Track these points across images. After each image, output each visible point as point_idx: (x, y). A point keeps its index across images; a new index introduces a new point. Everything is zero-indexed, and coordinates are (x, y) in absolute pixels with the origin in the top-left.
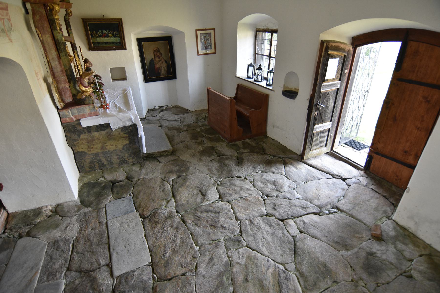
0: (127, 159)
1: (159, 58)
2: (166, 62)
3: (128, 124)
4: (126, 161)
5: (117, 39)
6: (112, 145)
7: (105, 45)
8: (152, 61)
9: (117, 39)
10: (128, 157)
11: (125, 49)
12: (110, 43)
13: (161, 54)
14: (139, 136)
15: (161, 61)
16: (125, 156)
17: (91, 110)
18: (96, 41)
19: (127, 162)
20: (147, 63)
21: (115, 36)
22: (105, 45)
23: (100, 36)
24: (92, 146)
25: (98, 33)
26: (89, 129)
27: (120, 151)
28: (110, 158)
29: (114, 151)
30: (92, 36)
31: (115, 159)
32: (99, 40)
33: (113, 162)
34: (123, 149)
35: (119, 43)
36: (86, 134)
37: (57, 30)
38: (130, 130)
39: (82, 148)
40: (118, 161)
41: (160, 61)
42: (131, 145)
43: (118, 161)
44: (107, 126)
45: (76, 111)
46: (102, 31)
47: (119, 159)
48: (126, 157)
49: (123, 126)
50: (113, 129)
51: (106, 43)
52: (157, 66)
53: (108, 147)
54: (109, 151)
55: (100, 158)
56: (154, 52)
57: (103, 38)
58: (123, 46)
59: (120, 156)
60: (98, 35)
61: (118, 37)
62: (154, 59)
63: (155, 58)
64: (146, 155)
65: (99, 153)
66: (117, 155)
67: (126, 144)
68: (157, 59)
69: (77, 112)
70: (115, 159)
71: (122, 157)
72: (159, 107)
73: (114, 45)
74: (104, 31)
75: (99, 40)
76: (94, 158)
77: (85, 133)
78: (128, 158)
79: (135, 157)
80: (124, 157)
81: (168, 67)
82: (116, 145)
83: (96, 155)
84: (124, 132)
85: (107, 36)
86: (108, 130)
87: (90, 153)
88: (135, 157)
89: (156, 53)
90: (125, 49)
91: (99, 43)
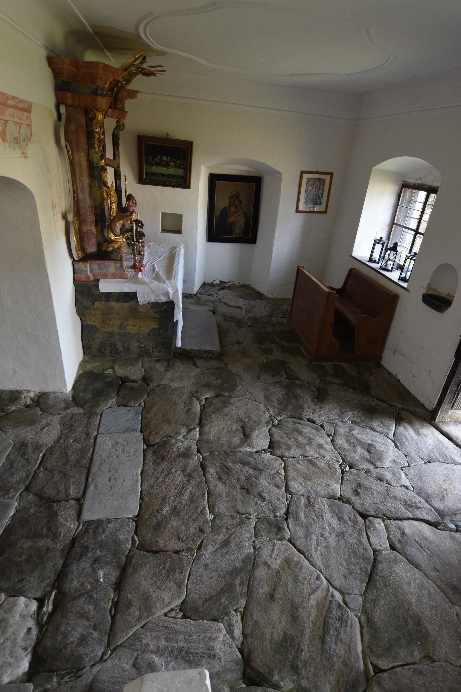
0: (151, 351)
1: (236, 208)
2: (245, 215)
3: (163, 299)
4: (149, 353)
5: (180, 172)
6: (134, 326)
7: (161, 178)
8: (224, 212)
9: (180, 172)
10: (152, 348)
11: (188, 187)
12: (169, 176)
13: (240, 202)
14: (175, 320)
15: (238, 213)
16: (149, 346)
17: (116, 269)
18: (150, 171)
19: (149, 355)
20: (217, 212)
21: (178, 167)
22: (161, 178)
23: (157, 165)
24: (108, 321)
25: (156, 159)
26: (108, 296)
27: (144, 336)
28: (128, 344)
29: (136, 334)
30: (146, 163)
31: (134, 346)
32: (155, 169)
33: (131, 350)
34: (149, 334)
35: (182, 177)
36: (103, 302)
37: (95, 148)
38: (164, 309)
39: (94, 321)
40: (139, 350)
41: (236, 212)
42: (161, 331)
43: (139, 350)
44: (132, 297)
45: (97, 267)
46: (161, 158)
47: (140, 347)
48: (150, 348)
49: (154, 301)
50: (141, 302)
51: (163, 175)
52: (231, 219)
53: (129, 327)
54: (129, 333)
55: (114, 340)
56: (231, 197)
57: (161, 168)
58: (186, 183)
59: (142, 343)
60: (155, 162)
61: (182, 168)
62: (228, 209)
63: (230, 207)
64: (180, 351)
65: (115, 332)
66: (139, 341)
67: (154, 329)
68: (233, 209)
69: (98, 269)
70: (134, 346)
71: (145, 346)
72: (221, 282)
73: (174, 180)
74: (164, 158)
75: (155, 169)
76: (106, 339)
77: (102, 300)
78: (152, 350)
79: (162, 350)
80: (148, 347)
81: (247, 223)
82: (140, 327)
83: (111, 334)
84: (155, 310)
85: (166, 165)
86: (133, 303)
87: (103, 330)
88: (162, 350)
89: (232, 200)
90: (188, 187)
91: (153, 174)
